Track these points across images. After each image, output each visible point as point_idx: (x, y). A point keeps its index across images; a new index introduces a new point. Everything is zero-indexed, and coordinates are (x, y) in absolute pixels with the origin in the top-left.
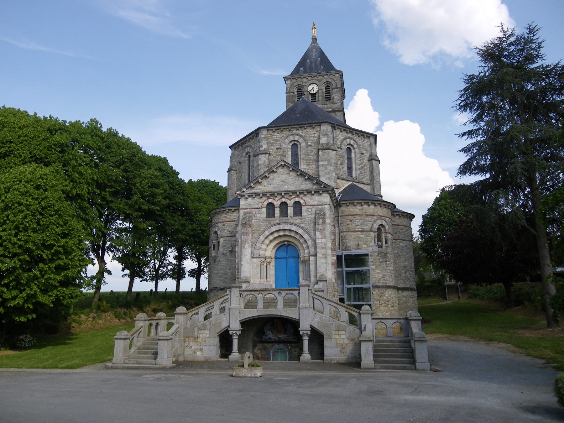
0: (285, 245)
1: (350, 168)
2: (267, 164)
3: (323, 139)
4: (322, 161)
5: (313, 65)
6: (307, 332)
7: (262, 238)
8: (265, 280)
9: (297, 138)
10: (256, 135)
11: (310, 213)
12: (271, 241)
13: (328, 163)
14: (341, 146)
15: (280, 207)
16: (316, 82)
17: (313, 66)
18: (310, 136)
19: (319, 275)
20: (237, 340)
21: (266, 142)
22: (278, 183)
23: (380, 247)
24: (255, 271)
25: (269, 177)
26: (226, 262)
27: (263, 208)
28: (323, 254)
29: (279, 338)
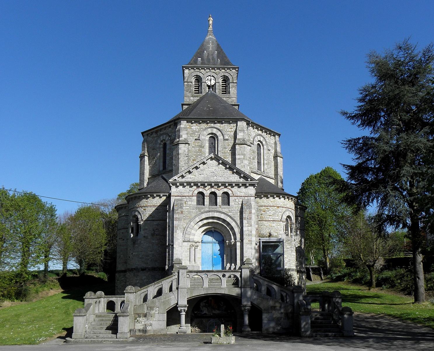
1: (259, 163)
2: (187, 153)
5: (211, 57)
6: (184, 308)
9: (215, 131)
10: (175, 124)
11: (237, 203)
14: (253, 142)
15: (209, 196)
17: (211, 58)
19: (245, 259)
20: (184, 315)
21: (186, 132)
23: (287, 235)
26: (148, 245)
27: (194, 196)
28: (249, 241)
29: (214, 314)
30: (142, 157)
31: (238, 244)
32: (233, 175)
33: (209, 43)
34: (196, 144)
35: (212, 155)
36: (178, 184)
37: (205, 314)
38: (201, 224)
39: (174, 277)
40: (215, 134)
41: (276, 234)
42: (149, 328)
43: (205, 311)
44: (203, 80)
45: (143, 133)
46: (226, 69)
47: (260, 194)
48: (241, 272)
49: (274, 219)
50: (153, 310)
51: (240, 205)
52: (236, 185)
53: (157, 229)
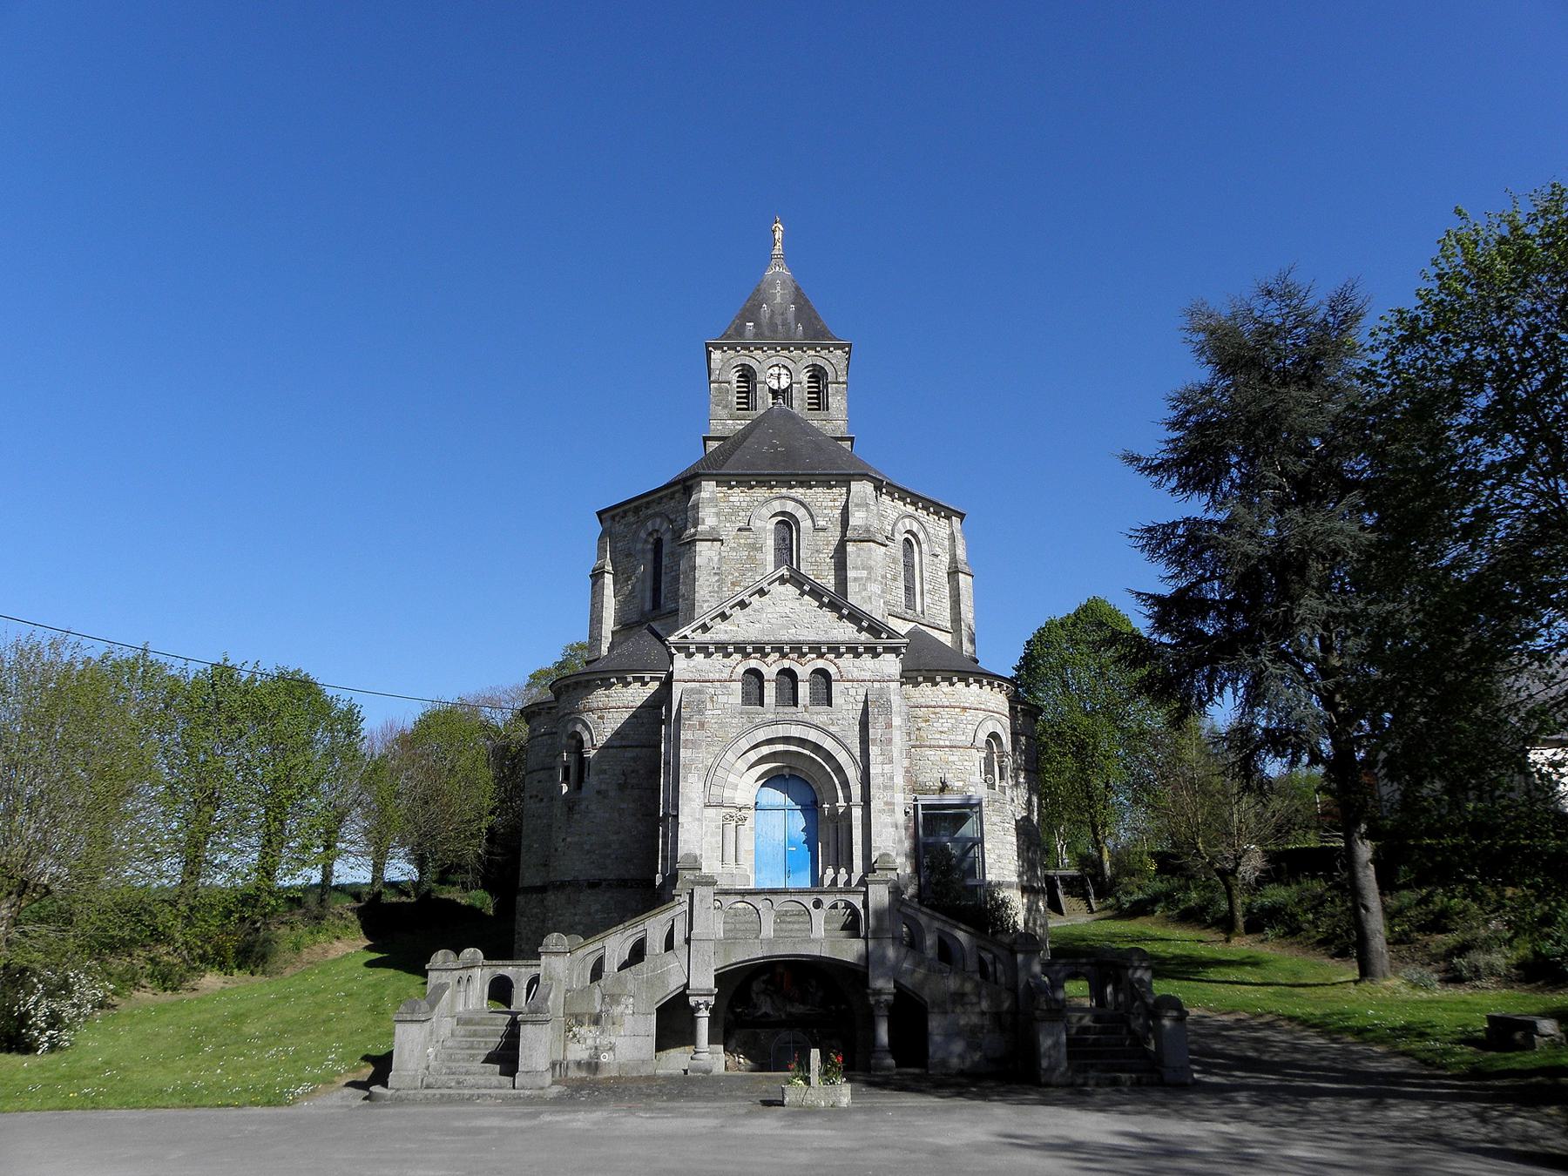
0: (783, 776)
1: (909, 590)
6: (705, 998)
7: (730, 756)
9: (790, 507)
10: (685, 490)
13: (869, 573)
14: (893, 535)
15: (776, 681)
16: (788, 363)
18: (824, 504)
19: (875, 855)
21: (714, 510)
23: (992, 786)
24: (713, 840)
26: (607, 815)
27: (735, 681)
28: (886, 803)
29: (790, 1014)
30: (597, 576)
31: (857, 813)
34: (742, 541)
35: (784, 571)
36: (693, 649)
37: (766, 1015)
39: (678, 909)
40: (791, 516)
41: (961, 784)
42: (605, 1058)
43: (765, 1007)
44: (760, 377)
45: (600, 514)
47: (915, 674)
48: (866, 894)
50: (619, 1004)
51: (861, 705)
53: (633, 772)
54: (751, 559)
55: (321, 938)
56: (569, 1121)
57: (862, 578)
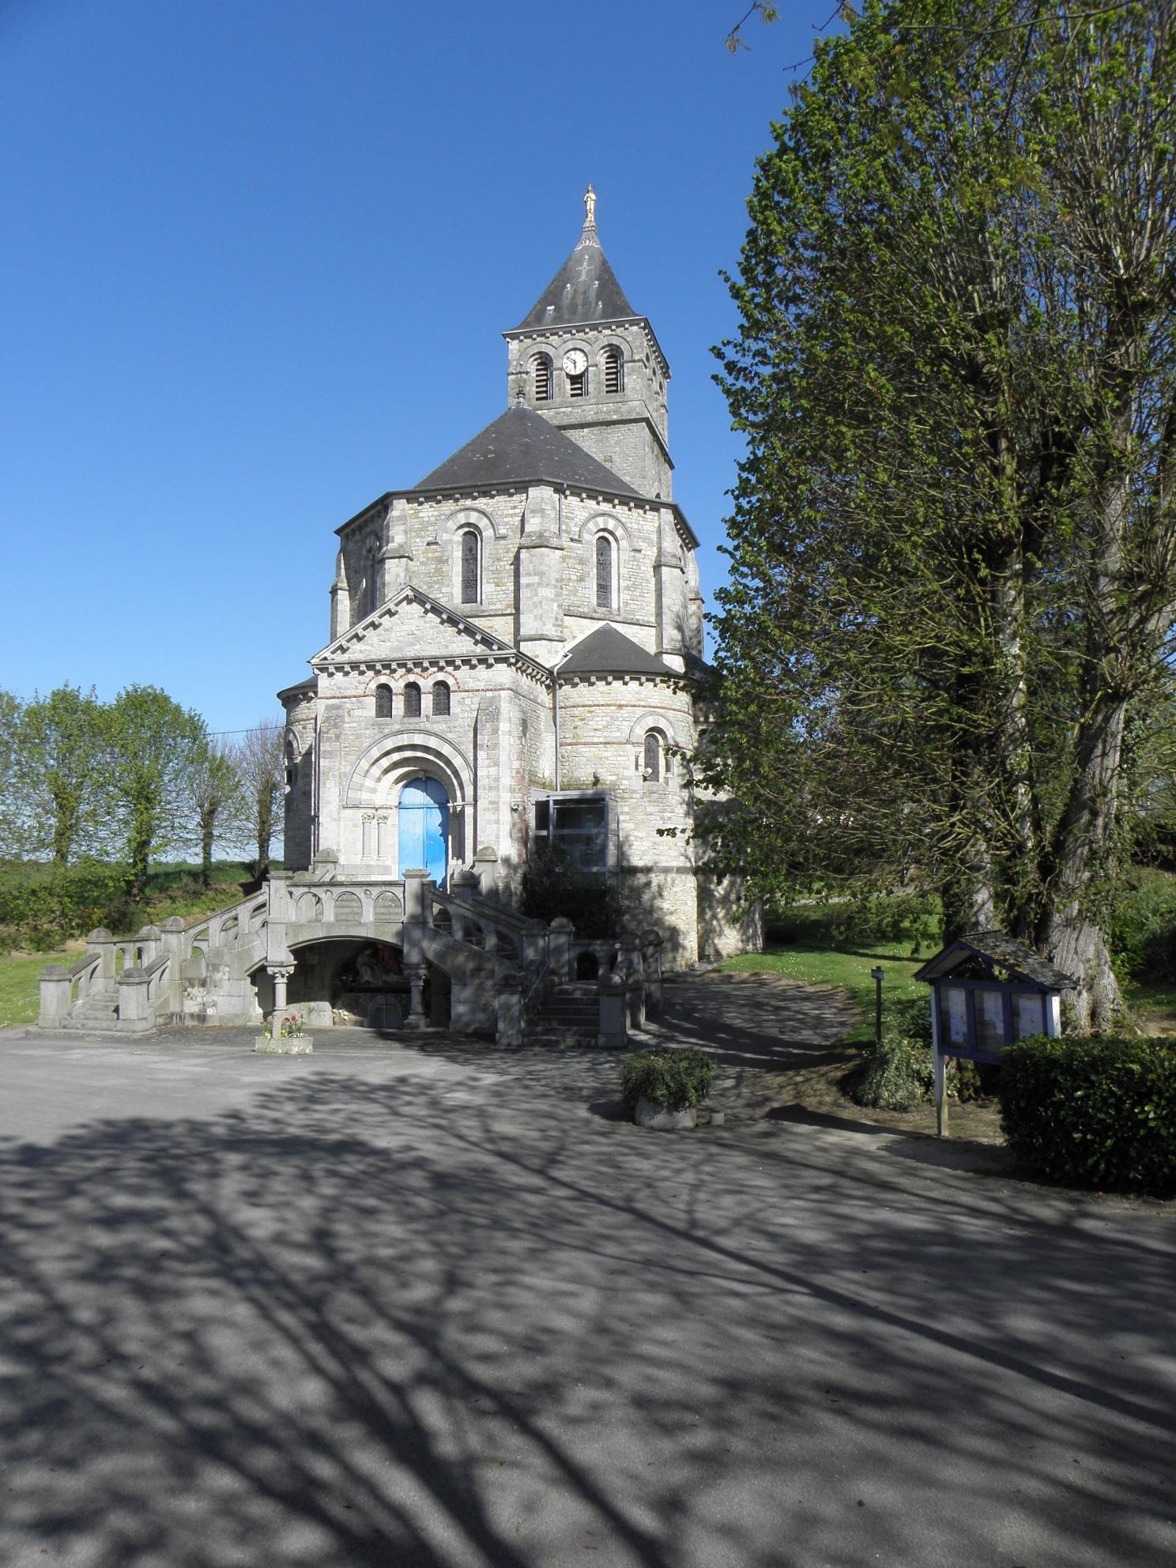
1: (603, 588)
3: (532, 521)
4: (528, 574)
8: (375, 857)
9: (474, 517)
11: (467, 709)
12: (387, 771)
18: (505, 512)
19: (479, 847)
21: (402, 528)
22: (401, 639)
25: (380, 624)
29: (386, 982)
30: (334, 592)
32: (459, 638)
33: (580, 261)
34: (430, 555)
36: (332, 669)
37: (368, 982)
38: (386, 762)
41: (614, 778)
42: (210, 1011)
43: (366, 976)
44: (556, 364)
46: (614, 327)
47: (571, 675)
49: (608, 740)
50: (218, 971)
52: (466, 662)
54: (439, 571)
55: (196, 910)
56: (103, 1055)
57: (533, 584)
